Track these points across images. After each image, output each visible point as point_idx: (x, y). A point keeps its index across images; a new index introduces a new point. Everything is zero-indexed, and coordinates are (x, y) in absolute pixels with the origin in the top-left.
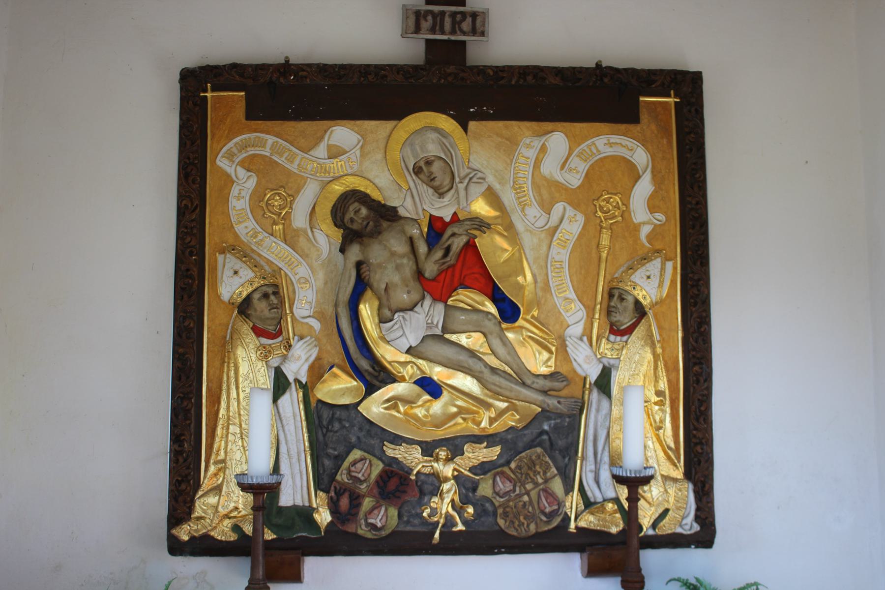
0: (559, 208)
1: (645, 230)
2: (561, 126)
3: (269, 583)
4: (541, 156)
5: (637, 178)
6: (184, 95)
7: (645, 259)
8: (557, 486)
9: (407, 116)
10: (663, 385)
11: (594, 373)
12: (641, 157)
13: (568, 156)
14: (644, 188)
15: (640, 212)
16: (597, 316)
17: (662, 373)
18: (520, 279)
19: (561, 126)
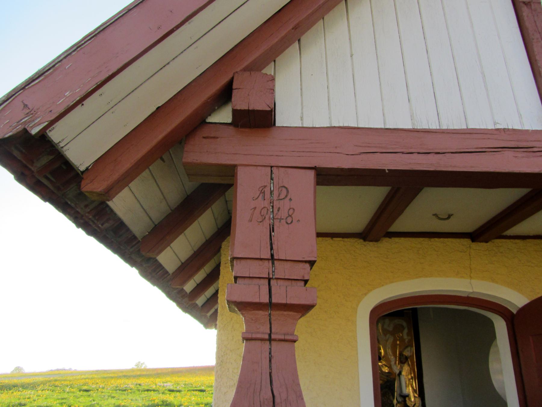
0: (388, 336)
1: (406, 340)
2: (154, 400)
3: (391, 191)
4: (270, 347)
5: (404, 329)
6: (107, 209)
7: (407, 347)
8: (391, 398)
9: (393, 170)
10: (412, 375)
11: (398, 372)
12: (405, 324)
13: (29, 384)
14: (406, 331)
15: (405, 337)
16: (397, 359)
17: (412, 372)
18: (381, 351)
19: (154, 400)
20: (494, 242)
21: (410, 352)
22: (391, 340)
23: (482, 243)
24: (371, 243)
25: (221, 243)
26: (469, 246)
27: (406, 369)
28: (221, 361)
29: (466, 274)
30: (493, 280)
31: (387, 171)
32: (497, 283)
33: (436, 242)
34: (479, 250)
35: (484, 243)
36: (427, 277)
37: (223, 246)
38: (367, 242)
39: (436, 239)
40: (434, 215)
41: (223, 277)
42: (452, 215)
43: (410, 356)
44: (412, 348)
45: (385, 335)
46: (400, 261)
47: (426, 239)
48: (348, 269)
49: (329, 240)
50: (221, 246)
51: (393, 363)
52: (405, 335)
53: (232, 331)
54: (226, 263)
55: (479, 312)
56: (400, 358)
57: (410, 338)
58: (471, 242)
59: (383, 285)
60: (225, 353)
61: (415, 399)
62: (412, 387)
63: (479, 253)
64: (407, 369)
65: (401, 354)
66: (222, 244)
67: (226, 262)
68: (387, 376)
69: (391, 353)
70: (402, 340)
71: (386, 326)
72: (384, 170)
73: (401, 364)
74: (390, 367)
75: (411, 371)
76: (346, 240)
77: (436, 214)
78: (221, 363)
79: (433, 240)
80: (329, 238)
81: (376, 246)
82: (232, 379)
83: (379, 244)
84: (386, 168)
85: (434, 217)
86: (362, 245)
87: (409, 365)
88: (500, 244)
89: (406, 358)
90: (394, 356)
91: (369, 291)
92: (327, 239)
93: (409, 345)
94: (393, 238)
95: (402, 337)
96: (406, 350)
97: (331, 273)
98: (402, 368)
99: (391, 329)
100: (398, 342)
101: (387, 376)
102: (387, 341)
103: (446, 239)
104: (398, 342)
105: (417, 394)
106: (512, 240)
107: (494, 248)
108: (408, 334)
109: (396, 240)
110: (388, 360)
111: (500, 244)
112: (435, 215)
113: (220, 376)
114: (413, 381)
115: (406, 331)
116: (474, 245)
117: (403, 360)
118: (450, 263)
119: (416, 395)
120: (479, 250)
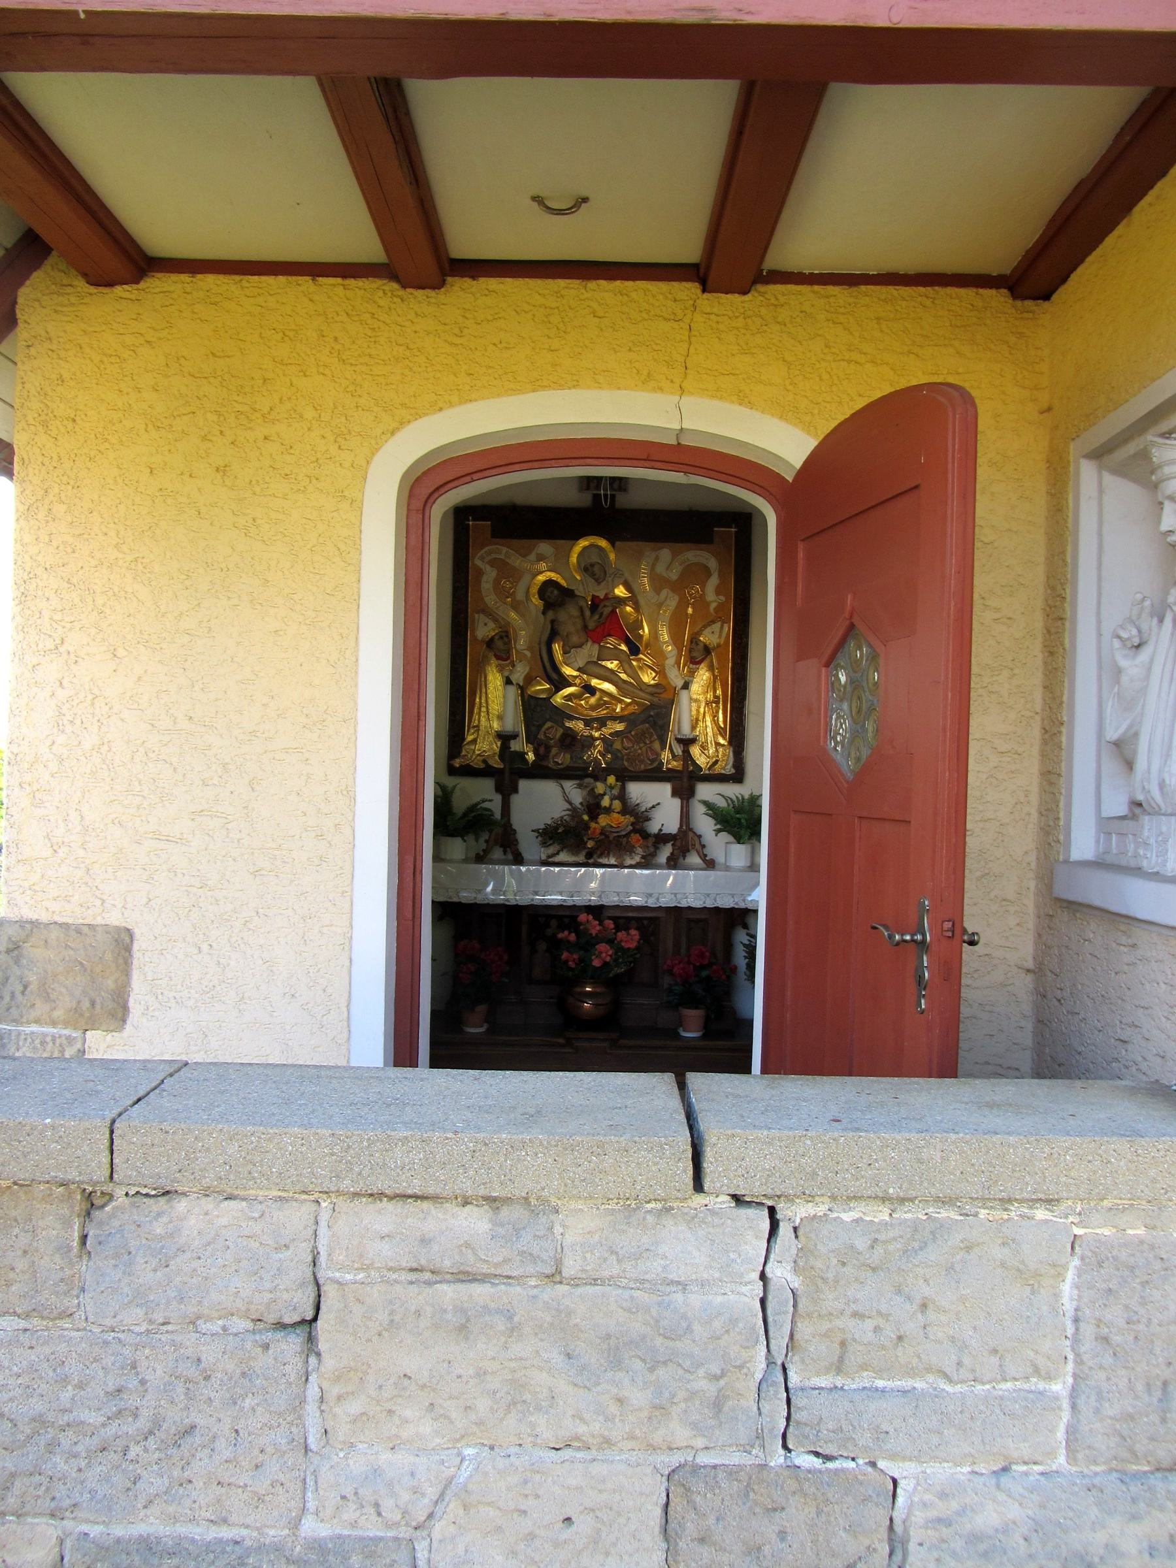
0: (665, 592)
1: (713, 605)
8: (657, 745)
10: (719, 692)
12: (713, 563)
14: (714, 581)
18: (641, 632)
20: (762, 294)
21: (717, 635)
22: (673, 602)
23: (729, 296)
24: (419, 293)
25: (17, 291)
26: (691, 302)
27: (703, 676)
28: (23, 593)
29: (672, 381)
30: (743, 399)
31: (82, 16)
32: (751, 405)
33: (603, 291)
34: (718, 315)
35: (736, 295)
36: (561, 387)
37: (20, 300)
38: (409, 290)
39: (603, 283)
40: (534, 199)
41: (23, 383)
42: (585, 200)
43: (719, 646)
44: (726, 626)
45: (657, 590)
46: (494, 344)
47: (575, 283)
48: (352, 365)
49: (305, 282)
50: (16, 298)
51: (670, 661)
52: (713, 592)
53: (47, 522)
54: (28, 346)
55: (739, 496)
56: (690, 651)
57: (722, 598)
58: (699, 291)
59: (441, 409)
60: (31, 576)
61: (717, 751)
62: (715, 721)
63: (718, 322)
64: (705, 678)
65: (694, 640)
66: (19, 293)
67: (30, 343)
68: (652, 694)
69: (666, 638)
70: (701, 602)
71: (660, 569)
72: (76, 13)
73: (691, 666)
74: (661, 672)
75: (715, 682)
76: (351, 282)
77: (538, 197)
78: (23, 598)
79: (592, 284)
80: (307, 278)
81: (433, 300)
82: (50, 636)
83: (440, 296)
84: (80, 8)
85: (535, 204)
86: (395, 300)
87: (711, 668)
88: (782, 300)
89: (707, 650)
90: (675, 644)
91: (403, 423)
92: (301, 279)
93: (719, 618)
94: (482, 280)
95: (702, 597)
96: (708, 630)
97: (305, 376)
98: (692, 673)
99: (674, 575)
100: (690, 610)
101: (652, 694)
102: (660, 605)
103: (630, 283)
104: (690, 610)
105: (724, 738)
106: (816, 288)
107: (763, 311)
108: (718, 592)
109: (493, 283)
110: (660, 655)
111: (782, 300)
112: (538, 200)
113: (20, 627)
114: (718, 707)
115: (714, 581)
116: (709, 302)
117: (697, 654)
118: (630, 350)
119: (722, 741)
120: (718, 315)
